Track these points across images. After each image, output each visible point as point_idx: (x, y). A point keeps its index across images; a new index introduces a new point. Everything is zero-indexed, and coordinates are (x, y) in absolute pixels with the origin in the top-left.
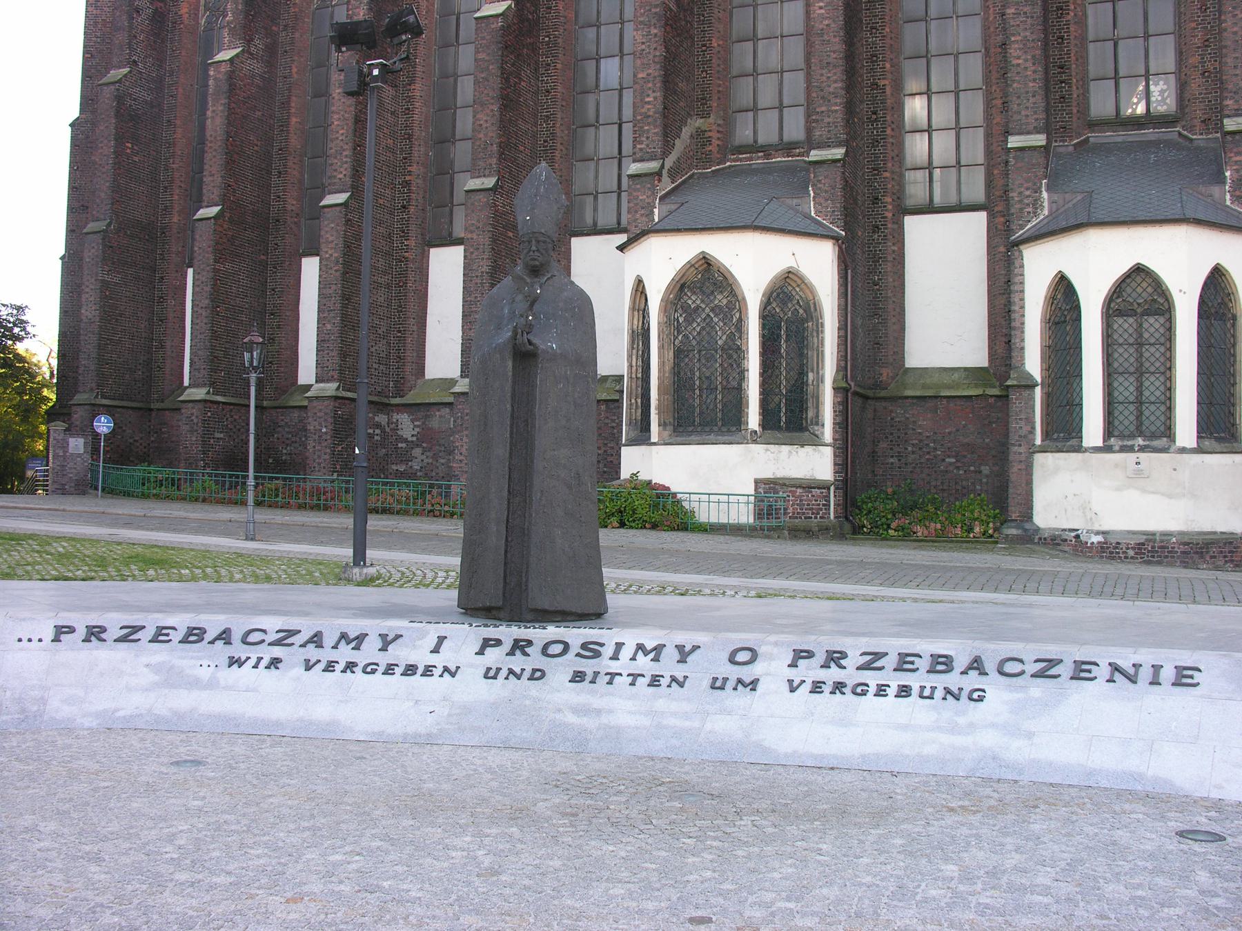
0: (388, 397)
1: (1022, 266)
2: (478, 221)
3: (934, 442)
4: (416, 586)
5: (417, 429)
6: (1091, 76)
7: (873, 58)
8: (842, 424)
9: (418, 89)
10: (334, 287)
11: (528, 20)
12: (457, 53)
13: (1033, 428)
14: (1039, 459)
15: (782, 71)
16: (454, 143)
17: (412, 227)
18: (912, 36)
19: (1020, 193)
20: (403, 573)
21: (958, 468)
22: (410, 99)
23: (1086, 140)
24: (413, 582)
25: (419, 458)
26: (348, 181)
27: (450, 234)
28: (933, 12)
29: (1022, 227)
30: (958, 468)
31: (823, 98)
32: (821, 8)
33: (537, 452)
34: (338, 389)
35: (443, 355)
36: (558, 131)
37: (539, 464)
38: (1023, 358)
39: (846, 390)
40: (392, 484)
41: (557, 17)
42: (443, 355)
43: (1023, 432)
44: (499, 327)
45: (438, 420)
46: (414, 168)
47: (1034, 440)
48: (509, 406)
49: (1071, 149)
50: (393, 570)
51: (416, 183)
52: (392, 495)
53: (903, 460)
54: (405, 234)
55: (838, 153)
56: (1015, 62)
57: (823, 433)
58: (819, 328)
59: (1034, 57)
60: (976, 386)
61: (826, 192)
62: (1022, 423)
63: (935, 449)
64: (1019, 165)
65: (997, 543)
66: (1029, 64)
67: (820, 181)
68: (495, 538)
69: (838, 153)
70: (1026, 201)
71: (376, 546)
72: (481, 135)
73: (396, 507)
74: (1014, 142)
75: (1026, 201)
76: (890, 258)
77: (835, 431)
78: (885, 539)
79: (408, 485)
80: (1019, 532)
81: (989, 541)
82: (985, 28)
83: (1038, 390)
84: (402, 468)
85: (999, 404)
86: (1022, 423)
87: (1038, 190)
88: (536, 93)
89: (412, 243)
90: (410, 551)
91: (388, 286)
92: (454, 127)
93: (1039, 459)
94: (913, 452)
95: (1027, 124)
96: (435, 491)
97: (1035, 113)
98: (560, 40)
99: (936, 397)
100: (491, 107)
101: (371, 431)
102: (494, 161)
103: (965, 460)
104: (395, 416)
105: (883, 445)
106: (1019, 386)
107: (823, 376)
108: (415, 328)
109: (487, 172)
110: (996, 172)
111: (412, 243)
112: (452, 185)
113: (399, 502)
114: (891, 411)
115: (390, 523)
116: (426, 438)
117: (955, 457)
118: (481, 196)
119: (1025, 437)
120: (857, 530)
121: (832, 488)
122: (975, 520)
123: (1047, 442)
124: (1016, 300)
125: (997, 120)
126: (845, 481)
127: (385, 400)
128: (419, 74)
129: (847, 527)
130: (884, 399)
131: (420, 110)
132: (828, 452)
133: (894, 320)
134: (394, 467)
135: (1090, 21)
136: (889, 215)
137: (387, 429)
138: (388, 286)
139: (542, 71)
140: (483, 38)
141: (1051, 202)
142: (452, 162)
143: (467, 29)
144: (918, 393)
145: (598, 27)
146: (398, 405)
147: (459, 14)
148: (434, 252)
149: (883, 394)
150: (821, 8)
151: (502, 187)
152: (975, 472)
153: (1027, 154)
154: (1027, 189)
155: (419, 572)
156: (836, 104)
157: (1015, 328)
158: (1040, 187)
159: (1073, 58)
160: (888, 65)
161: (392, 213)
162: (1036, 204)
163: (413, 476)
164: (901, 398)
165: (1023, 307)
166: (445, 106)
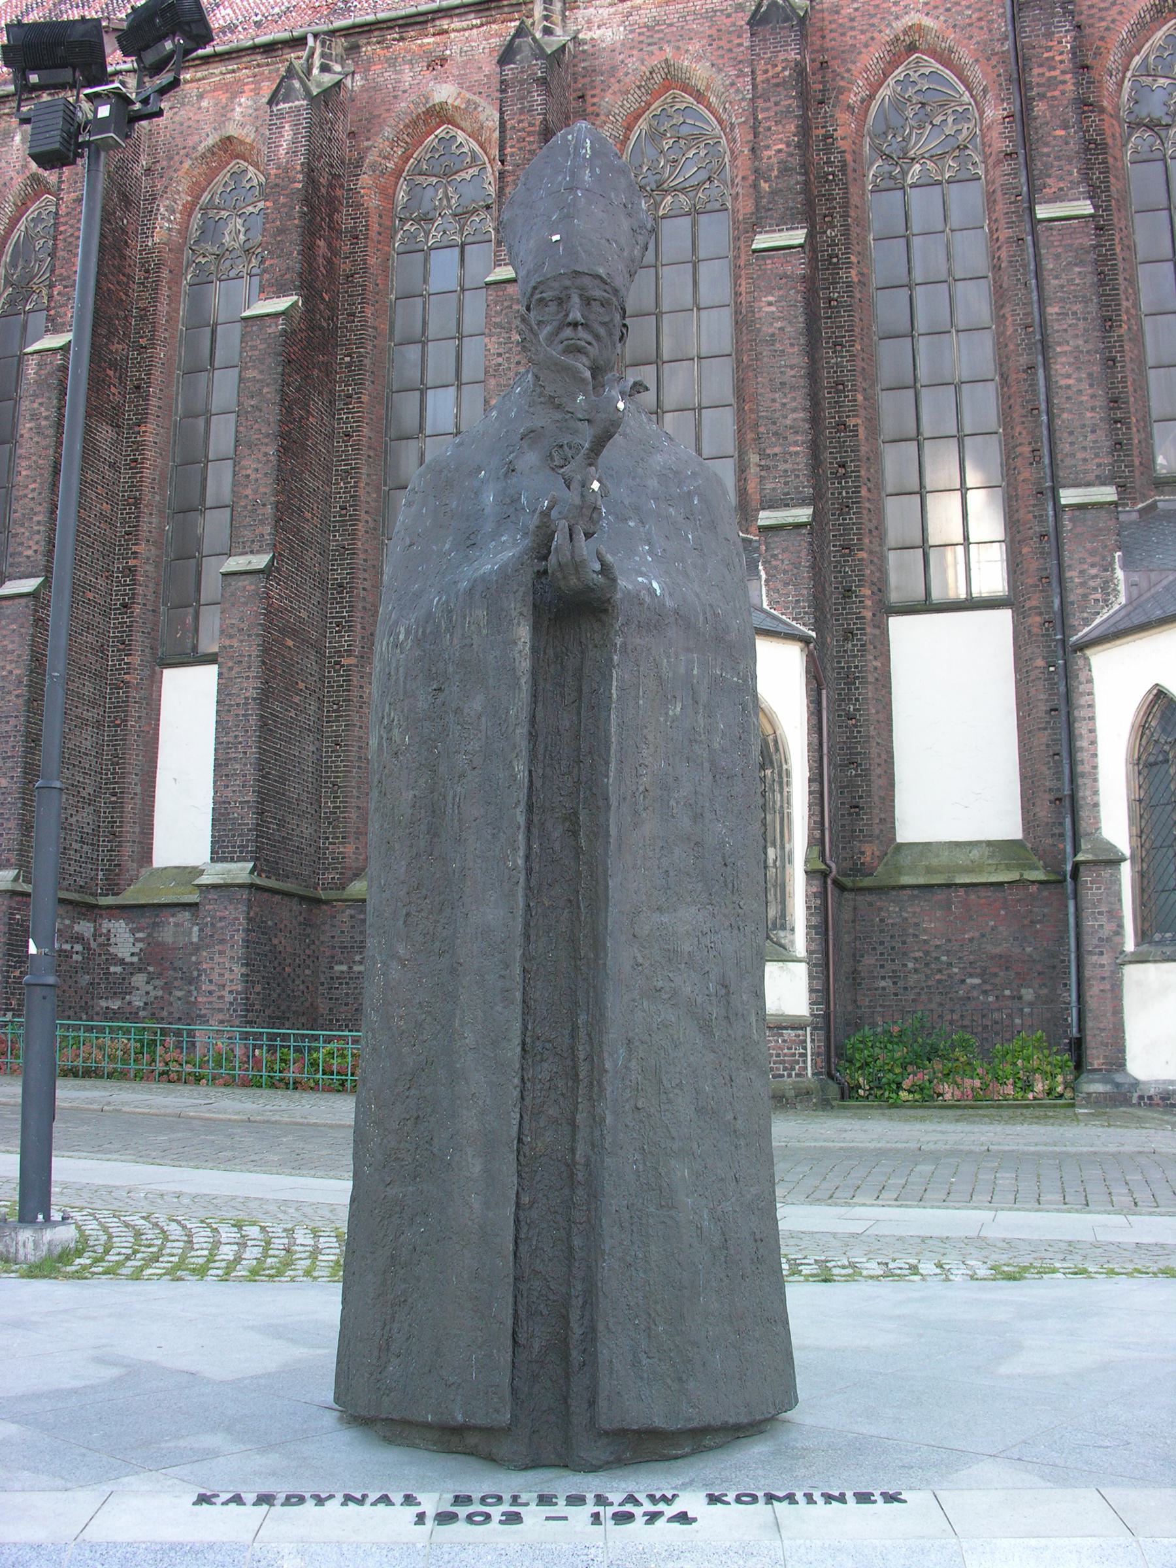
0: (95, 895)
1: (1090, 681)
2: (241, 619)
3: (948, 953)
4: (174, 1274)
5: (140, 945)
6: (1154, 416)
7: (839, 386)
8: (821, 928)
9: (152, 432)
10: (13, 721)
11: (321, 328)
12: (211, 380)
13: (1121, 926)
14: (1133, 974)
15: (701, 408)
16: (203, 513)
17: (138, 636)
18: (891, 358)
19: (1082, 572)
20: (138, 1234)
21: (985, 992)
22: (139, 447)
23: (1154, 506)
24: (166, 1262)
25: (142, 988)
26: (41, 560)
27: (195, 648)
28: (921, 325)
29: (1087, 622)
30: (985, 992)
31: (776, 434)
32: (770, 304)
33: (613, 914)
34: (16, 879)
35: (183, 825)
36: (361, 492)
37: (621, 956)
38: (1097, 819)
39: (824, 875)
40: (102, 1030)
41: (363, 328)
42: (183, 825)
43: (1106, 932)
44: (470, 542)
45: (176, 931)
46: (142, 548)
47: (1123, 944)
48: (520, 769)
49: (1134, 516)
50: (112, 1223)
51: (146, 570)
52: (101, 1048)
53: (901, 984)
54: (125, 646)
55: (804, 514)
56: (1063, 382)
57: (792, 942)
58: (783, 778)
59: (1090, 375)
60: (1008, 867)
61: (785, 572)
62: (1103, 920)
63: (950, 965)
64: (1079, 530)
65: (1073, 1106)
66: (1084, 386)
67: (775, 556)
68: (479, 1193)
69: (804, 514)
70: (1092, 583)
71: (73, 1148)
72: (248, 492)
73: (107, 1066)
74: (1068, 496)
75: (1092, 583)
76: (871, 679)
77: (810, 939)
78: (894, 1106)
79: (127, 1031)
80: (1108, 1088)
81: (1060, 1104)
82: (1000, 345)
83: (1126, 870)
84: (115, 1005)
85: (1045, 893)
86: (1103, 920)
87: (1109, 567)
88: (330, 437)
89: (136, 660)
90: (142, 1157)
91: (99, 725)
92: (204, 488)
93: (1133, 974)
94: (916, 971)
95: (1085, 472)
96: (171, 1040)
97: (1097, 455)
98: (367, 361)
99: (948, 886)
100: (264, 449)
101: (67, 947)
102: (267, 530)
103: (997, 981)
104: (106, 925)
105: (869, 960)
106: (1095, 863)
107: (791, 853)
108: (138, 789)
109: (256, 547)
110: (1025, 550)
111: (136, 660)
112: (199, 574)
113: (112, 1058)
114: (880, 909)
115: (95, 1094)
116: (154, 958)
117: (981, 976)
118: (245, 582)
119: (1109, 940)
120: (848, 1093)
121: (808, 1029)
122: (1035, 1071)
123: (1145, 947)
124: (1084, 731)
125: (1026, 474)
126: (827, 1016)
127: (91, 900)
128: (153, 410)
129: (833, 1089)
130: (870, 890)
131: (153, 463)
132: (801, 970)
133: (879, 771)
134: (103, 1003)
135: (1149, 339)
136: (868, 614)
137: (93, 945)
138: (99, 725)
139: (339, 404)
140: (254, 348)
141: (1131, 585)
142: (200, 541)
143: (229, 340)
144: (921, 881)
145: (424, 344)
146: (109, 907)
147: (216, 324)
148: (168, 674)
149: (867, 882)
150: (770, 304)
151: (278, 570)
152: (1013, 998)
153: (1090, 514)
154: (1093, 565)
155: (174, 1229)
156: (796, 443)
157: (1083, 775)
158: (1112, 563)
159: (1131, 389)
160: (860, 397)
161: (105, 614)
162: (1107, 587)
163: (133, 1016)
164: (893, 888)
165: (1093, 742)
166: (191, 459)
